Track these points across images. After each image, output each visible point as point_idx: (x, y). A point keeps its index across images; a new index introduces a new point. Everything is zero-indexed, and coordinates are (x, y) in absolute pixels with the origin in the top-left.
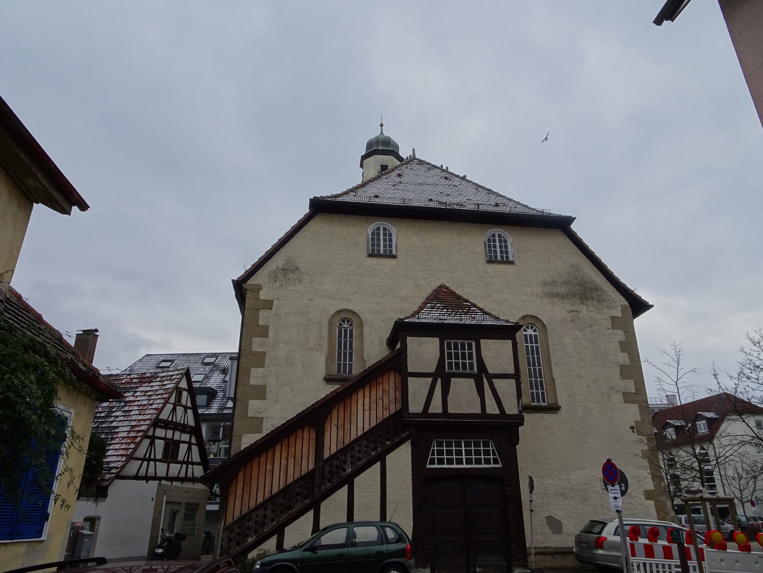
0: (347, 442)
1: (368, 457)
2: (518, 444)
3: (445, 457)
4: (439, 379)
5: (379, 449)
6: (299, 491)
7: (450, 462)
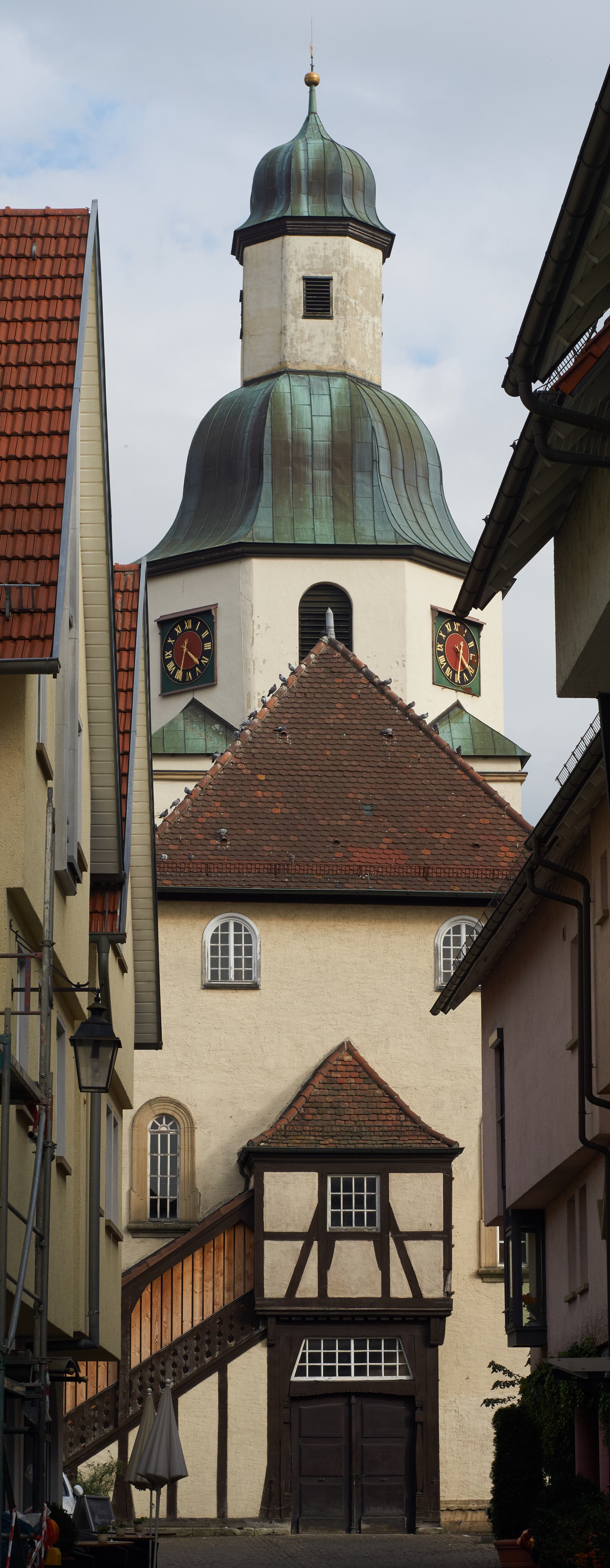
0: (167, 1341)
1: (199, 1366)
2: (442, 1344)
3: (322, 1364)
4: (316, 1243)
5: (217, 1353)
6: (96, 1415)
7: (330, 1371)
